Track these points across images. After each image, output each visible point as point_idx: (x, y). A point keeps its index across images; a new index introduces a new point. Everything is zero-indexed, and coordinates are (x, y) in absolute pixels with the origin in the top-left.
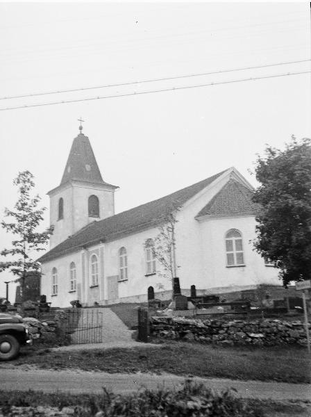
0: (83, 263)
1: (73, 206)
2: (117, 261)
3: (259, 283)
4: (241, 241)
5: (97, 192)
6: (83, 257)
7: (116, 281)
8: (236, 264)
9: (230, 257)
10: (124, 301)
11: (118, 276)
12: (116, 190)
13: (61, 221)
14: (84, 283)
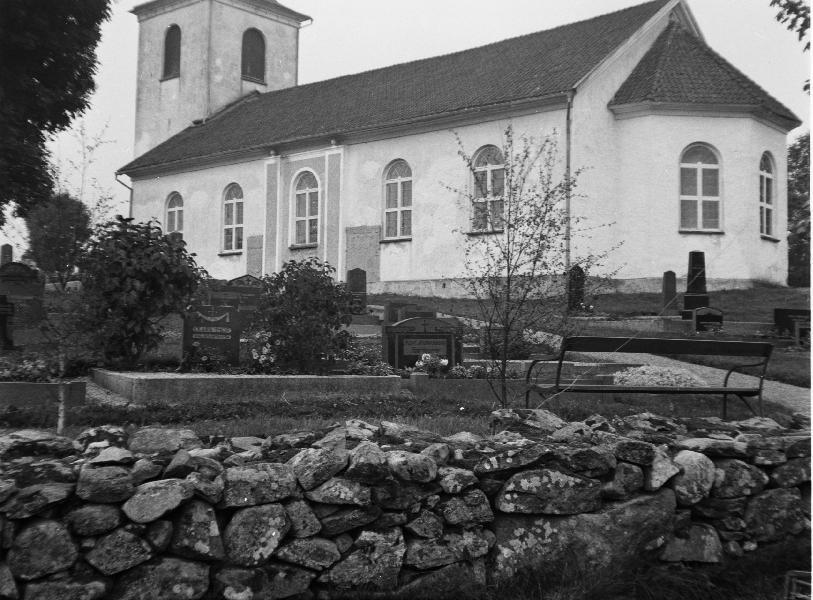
0: (271, 189)
1: (209, 49)
2: (380, 192)
3: (755, 277)
4: (715, 172)
5: (263, 23)
6: (272, 179)
7: (376, 240)
8: (700, 228)
9: (687, 210)
10: (393, 289)
11: (380, 228)
12: (303, 23)
13: (173, 83)
14: (272, 237)
